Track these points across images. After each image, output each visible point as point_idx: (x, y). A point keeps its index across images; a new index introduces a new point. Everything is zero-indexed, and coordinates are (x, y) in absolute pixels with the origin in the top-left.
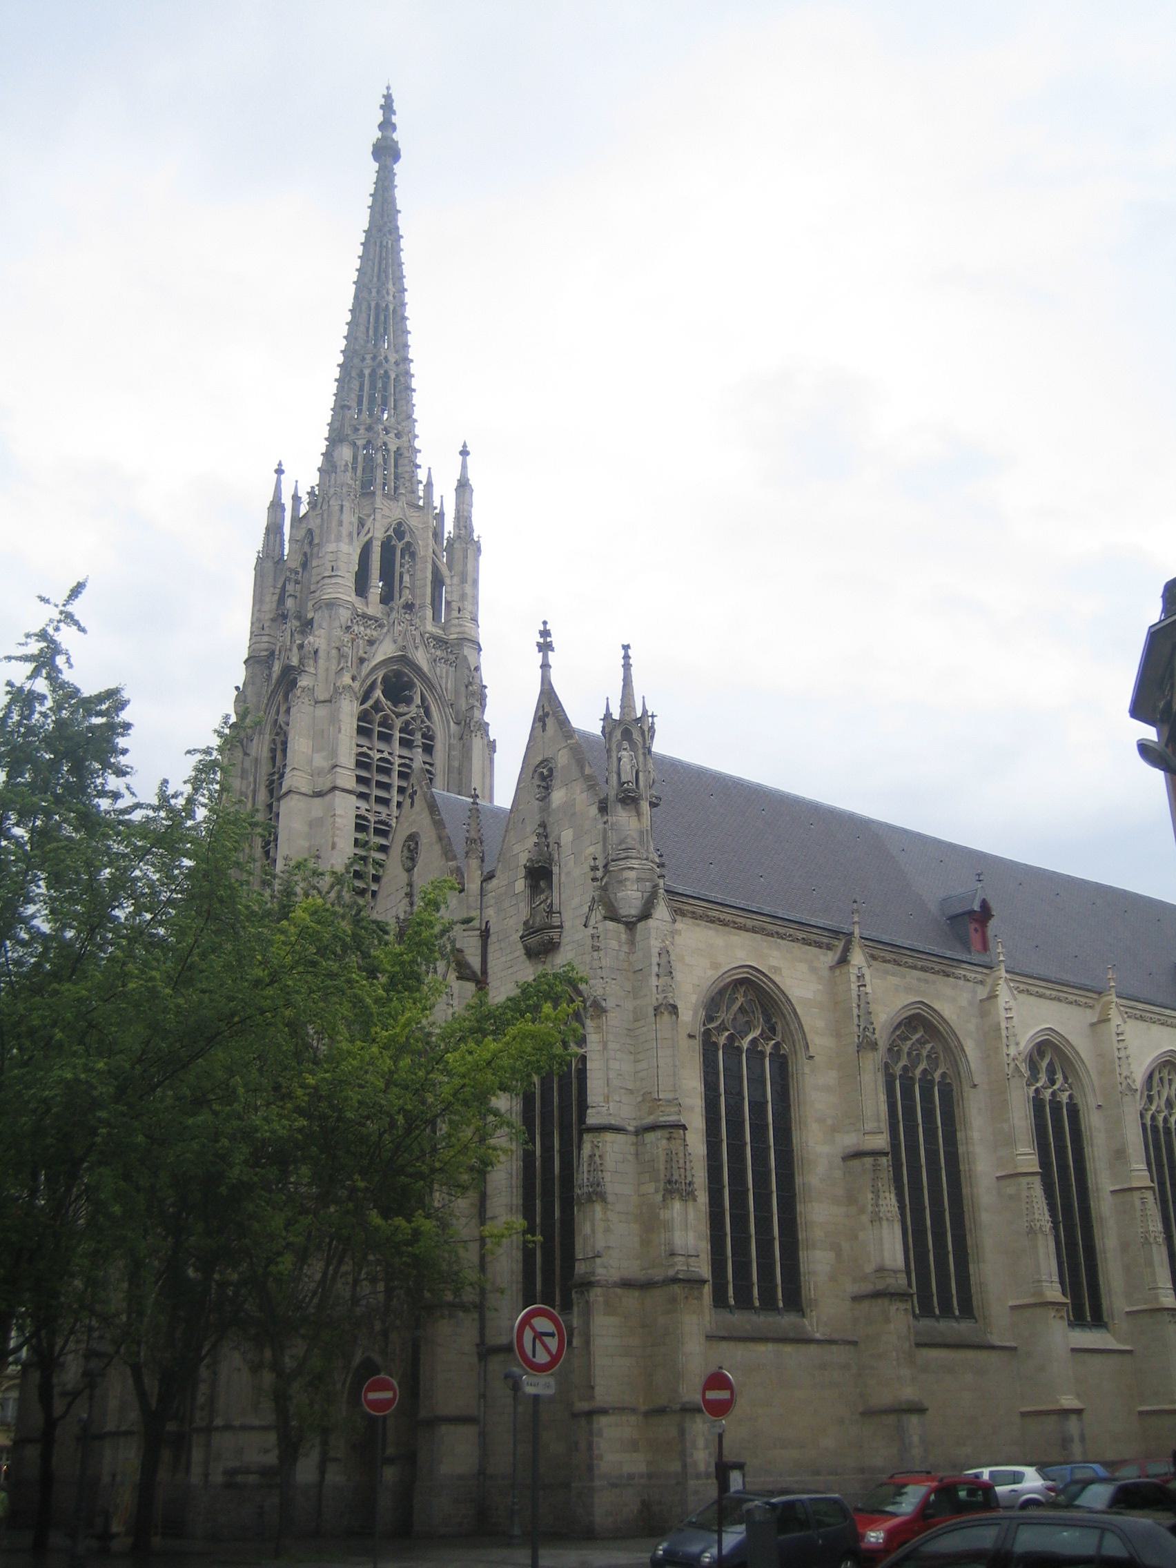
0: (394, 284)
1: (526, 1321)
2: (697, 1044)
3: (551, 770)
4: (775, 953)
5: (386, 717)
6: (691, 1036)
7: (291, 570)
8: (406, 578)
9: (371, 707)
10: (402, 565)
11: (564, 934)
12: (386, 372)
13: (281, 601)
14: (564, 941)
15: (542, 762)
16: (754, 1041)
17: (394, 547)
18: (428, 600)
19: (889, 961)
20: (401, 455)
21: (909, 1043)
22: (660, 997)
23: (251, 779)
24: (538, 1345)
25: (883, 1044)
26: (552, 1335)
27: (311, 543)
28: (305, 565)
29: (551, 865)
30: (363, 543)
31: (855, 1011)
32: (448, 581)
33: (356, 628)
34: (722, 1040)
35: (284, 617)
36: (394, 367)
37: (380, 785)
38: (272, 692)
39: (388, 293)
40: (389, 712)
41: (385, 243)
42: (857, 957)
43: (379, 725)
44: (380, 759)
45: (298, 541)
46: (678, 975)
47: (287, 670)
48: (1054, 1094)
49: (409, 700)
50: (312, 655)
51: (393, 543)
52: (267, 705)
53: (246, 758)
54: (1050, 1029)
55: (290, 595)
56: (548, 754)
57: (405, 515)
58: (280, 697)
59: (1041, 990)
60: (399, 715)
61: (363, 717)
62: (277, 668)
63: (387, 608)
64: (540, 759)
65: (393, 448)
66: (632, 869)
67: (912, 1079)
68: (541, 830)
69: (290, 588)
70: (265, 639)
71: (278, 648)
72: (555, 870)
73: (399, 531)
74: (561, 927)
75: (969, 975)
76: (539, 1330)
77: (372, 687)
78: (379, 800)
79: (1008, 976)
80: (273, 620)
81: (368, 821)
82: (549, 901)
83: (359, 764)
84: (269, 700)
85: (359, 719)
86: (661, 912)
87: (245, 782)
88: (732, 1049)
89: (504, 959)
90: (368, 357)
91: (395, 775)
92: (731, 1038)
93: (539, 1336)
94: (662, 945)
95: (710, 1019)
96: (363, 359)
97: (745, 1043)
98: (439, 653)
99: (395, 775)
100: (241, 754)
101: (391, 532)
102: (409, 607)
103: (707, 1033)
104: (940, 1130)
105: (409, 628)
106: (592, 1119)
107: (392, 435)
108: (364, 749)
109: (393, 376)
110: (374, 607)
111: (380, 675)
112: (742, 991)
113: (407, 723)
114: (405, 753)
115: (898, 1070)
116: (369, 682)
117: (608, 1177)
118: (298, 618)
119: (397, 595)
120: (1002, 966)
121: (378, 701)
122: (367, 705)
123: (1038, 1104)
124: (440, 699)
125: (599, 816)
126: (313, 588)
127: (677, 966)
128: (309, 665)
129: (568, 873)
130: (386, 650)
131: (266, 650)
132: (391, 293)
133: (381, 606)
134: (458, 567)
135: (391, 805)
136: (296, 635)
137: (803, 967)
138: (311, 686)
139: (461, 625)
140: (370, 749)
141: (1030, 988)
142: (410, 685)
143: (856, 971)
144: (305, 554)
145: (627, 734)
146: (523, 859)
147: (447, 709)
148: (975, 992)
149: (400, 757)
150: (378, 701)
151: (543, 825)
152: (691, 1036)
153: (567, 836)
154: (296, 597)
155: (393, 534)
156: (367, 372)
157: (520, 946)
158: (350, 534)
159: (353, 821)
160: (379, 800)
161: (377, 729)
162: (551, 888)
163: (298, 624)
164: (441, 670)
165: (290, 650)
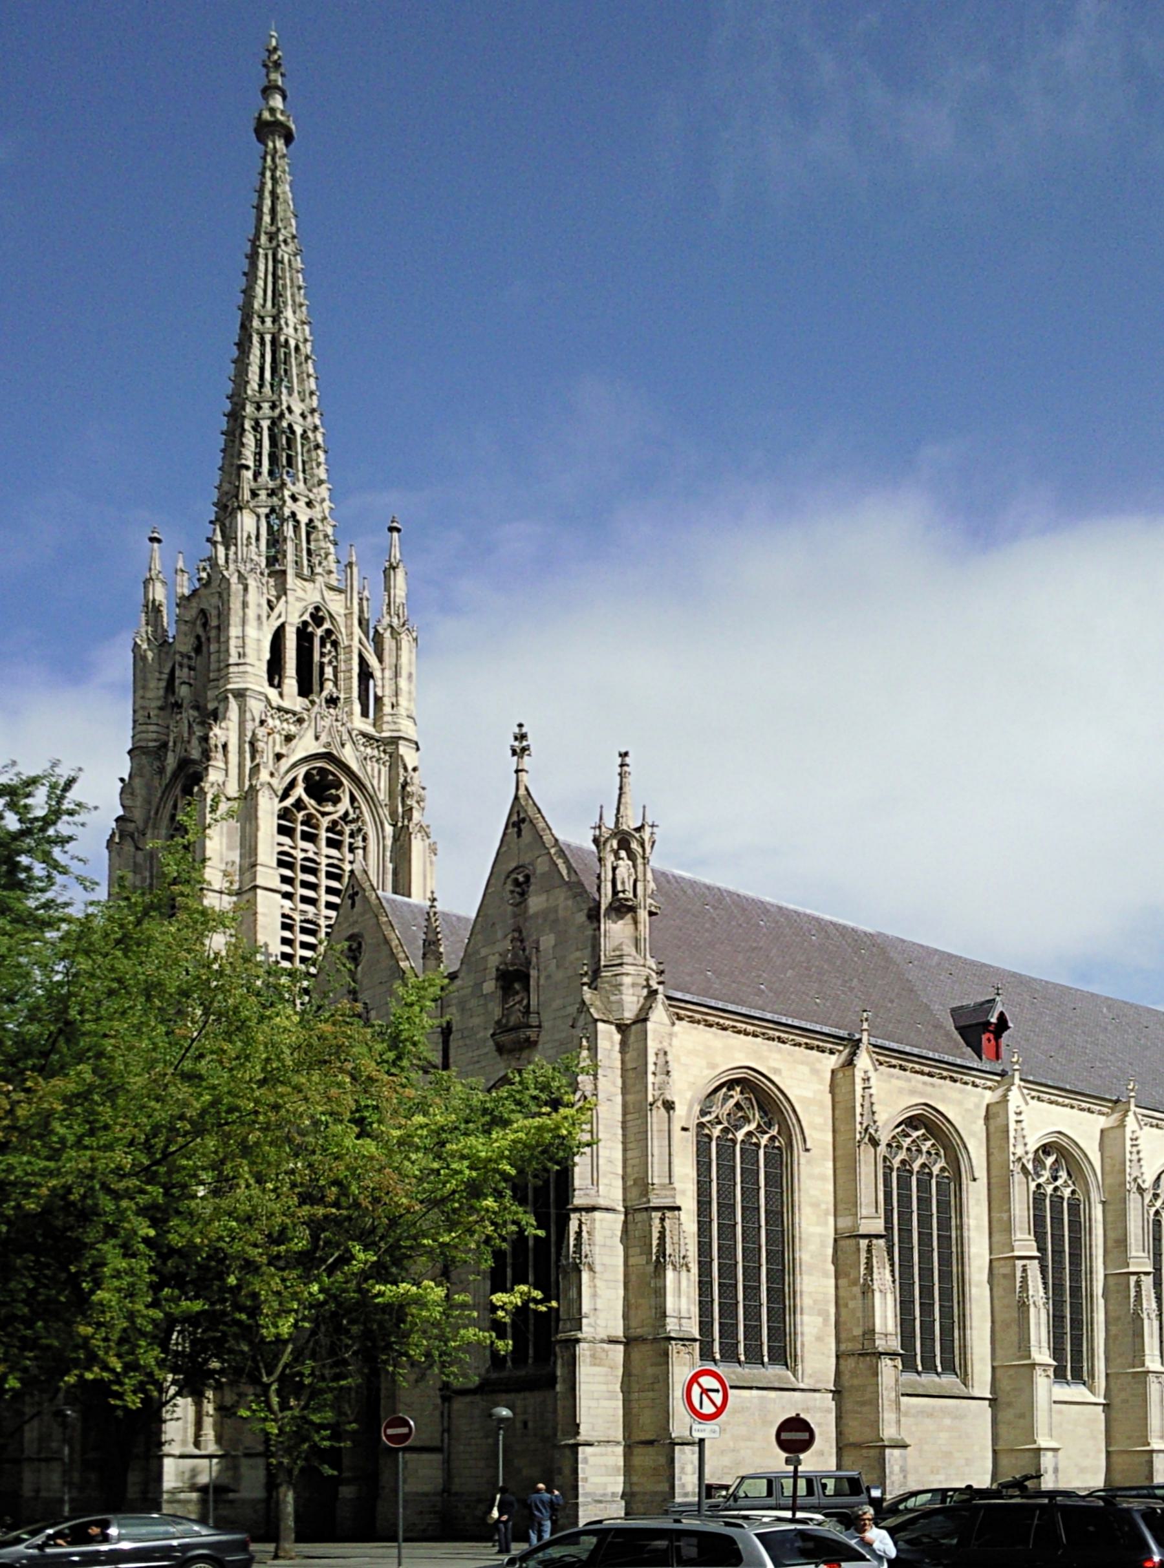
0: (294, 312)
1: (694, 1379)
2: (691, 1136)
3: (527, 877)
4: (777, 1056)
5: (310, 816)
6: (684, 1129)
7: (182, 655)
8: (329, 671)
9: (293, 805)
10: (322, 655)
11: (543, 1033)
12: (290, 426)
13: (170, 688)
14: (542, 1039)
15: (516, 868)
16: (749, 1134)
17: (312, 635)
18: (355, 694)
19: (894, 1066)
20: (314, 527)
21: (909, 1140)
22: (657, 1093)
23: (147, 874)
24: (704, 1397)
25: (884, 1137)
26: (717, 1391)
27: (205, 625)
28: (198, 649)
29: (528, 968)
30: (274, 629)
31: (858, 1110)
32: (377, 674)
33: (270, 721)
34: (716, 1131)
35: (178, 706)
36: (300, 420)
37: (305, 885)
38: (167, 786)
39: (287, 324)
40: (313, 811)
41: (279, 257)
42: (863, 1061)
43: (303, 823)
44: (305, 859)
45: (186, 622)
46: (674, 1074)
47: (184, 763)
48: (1056, 1189)
49: (336, 800)
50: (220, 749)
51: (310, 629)
52: (161, 799)
53: (140, 853)
54: (1060, 1133)
55: (184, 683)
56: (526, 859)
57: (323, 599)
58: (178, 791)
59: (1053, 1098)
60: (324, 814)
61: (284, 814)
62: (171, 761)
63: (306, 701)
64: (513, 865)
65: (303, 519)
66: (628, 974)
67: (911, 1172)
68: (516, 935)
69: (182, 674)
70: (153, 728)
71: (171, 739)
72: (533, 973)
73: (318, 620)
74: (539, 1026)
75: (978, 1081)
76: (706, 1386)
77: (292, 784)
78: (305, 900)
79: (1022, 1084)
80: (161, 708)
81: (293, 920)
82: (525, 1002)
83: (281, 864)
84: (163, 793)
85: (280, 817)
86: (659, 1015)
87: (138, 877)
88: (727, 1149)
89: (470, 1054)
90: (266, 405)
91: (323, 875)
92: (725, 1130)
93: (705, 1391)
94: (660, 1046)
95: (703, 1113)
96: (259, 408)
97: (740, 1135)
98: (369, 750)
99: (323, 875)
100: (133, 849)
101: (307, 617)
102: (332, 701)
103: (701, 1126)
104: (935, 1217)
105: (335, 724)
106: (578, 1200)
107: (302, 503)
108: (286, 849)
109: (299, 431)
110: (293, 700)
111: (302, 771)
112: (738, 1089)
113: (335, 823)
114: (334, 852)
115: (896, 1163)
116: (288, 779)
117: (597, 1250)
118: (197, 707)
119: (316, 687)
120: (1017, 1074)
121: (299, 800)
122: (288, 802)
123: (1038, 1198)
124: (371, 800)
125: (587, 923)
126: (212, 676)
127: (673, 1066)
128: (216, 759)
129: (548, 977)
130: (306, 745)
131: (155, 740)
132: (291, 324)
133: (300, 699)
134: (388, 658)
135: (318, 904)
136: (194, 725)
137: (805, 1069)
138: (221, 782)
139: (395, 723)
140: (291, 847)
141: (1041, 1095)
142: (339, 785)
143: (862, 1075)
144: (198, 637)
145: (624, 844)
146: (494, 961)
147: (380, 810)
148: (983, 1097)
149: (328, 857)
150: (299, 800)
151: (519, 930)
152: (684, 1129)
153: (547, 941)
154: (190, 685)
155: (309, 620)
156: (265, 424)
157: (491, 1043)
158: (259, 617)
159: (279, 920)
160: (305, 900)
161: (300, 828)
162: (528, 991)
163: (196, 714)
164: (373, 770)
165: (189, 742)
